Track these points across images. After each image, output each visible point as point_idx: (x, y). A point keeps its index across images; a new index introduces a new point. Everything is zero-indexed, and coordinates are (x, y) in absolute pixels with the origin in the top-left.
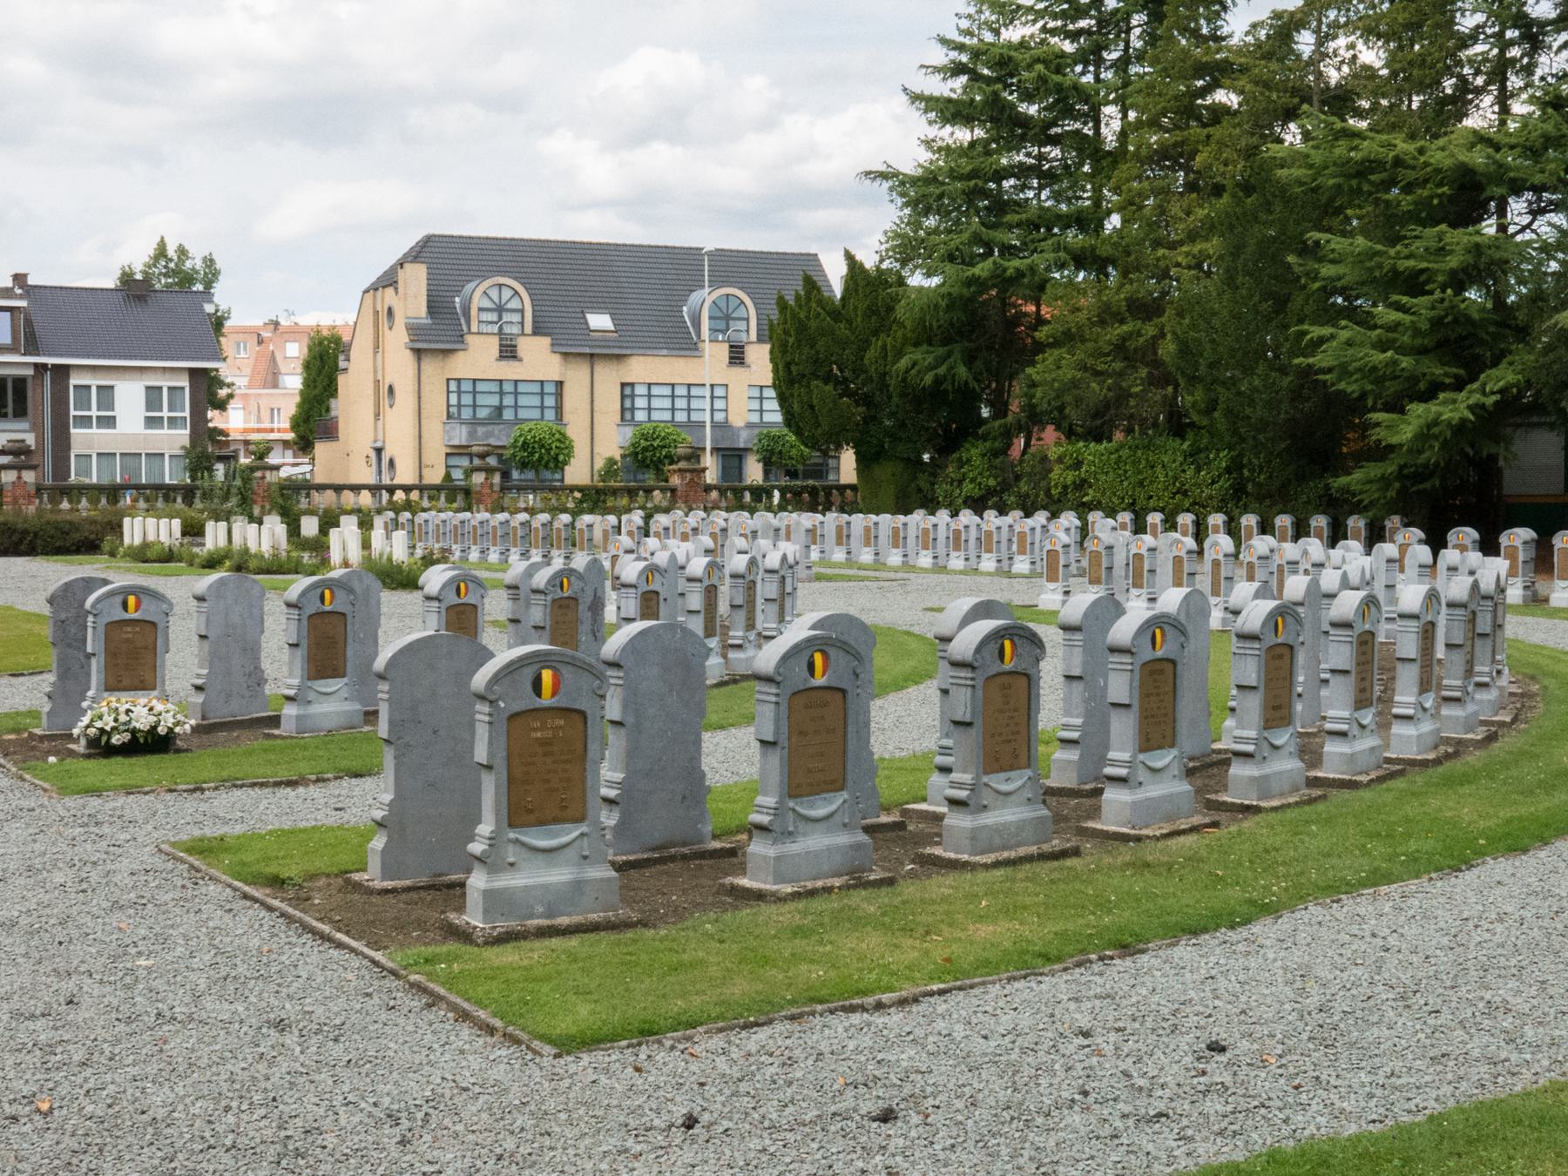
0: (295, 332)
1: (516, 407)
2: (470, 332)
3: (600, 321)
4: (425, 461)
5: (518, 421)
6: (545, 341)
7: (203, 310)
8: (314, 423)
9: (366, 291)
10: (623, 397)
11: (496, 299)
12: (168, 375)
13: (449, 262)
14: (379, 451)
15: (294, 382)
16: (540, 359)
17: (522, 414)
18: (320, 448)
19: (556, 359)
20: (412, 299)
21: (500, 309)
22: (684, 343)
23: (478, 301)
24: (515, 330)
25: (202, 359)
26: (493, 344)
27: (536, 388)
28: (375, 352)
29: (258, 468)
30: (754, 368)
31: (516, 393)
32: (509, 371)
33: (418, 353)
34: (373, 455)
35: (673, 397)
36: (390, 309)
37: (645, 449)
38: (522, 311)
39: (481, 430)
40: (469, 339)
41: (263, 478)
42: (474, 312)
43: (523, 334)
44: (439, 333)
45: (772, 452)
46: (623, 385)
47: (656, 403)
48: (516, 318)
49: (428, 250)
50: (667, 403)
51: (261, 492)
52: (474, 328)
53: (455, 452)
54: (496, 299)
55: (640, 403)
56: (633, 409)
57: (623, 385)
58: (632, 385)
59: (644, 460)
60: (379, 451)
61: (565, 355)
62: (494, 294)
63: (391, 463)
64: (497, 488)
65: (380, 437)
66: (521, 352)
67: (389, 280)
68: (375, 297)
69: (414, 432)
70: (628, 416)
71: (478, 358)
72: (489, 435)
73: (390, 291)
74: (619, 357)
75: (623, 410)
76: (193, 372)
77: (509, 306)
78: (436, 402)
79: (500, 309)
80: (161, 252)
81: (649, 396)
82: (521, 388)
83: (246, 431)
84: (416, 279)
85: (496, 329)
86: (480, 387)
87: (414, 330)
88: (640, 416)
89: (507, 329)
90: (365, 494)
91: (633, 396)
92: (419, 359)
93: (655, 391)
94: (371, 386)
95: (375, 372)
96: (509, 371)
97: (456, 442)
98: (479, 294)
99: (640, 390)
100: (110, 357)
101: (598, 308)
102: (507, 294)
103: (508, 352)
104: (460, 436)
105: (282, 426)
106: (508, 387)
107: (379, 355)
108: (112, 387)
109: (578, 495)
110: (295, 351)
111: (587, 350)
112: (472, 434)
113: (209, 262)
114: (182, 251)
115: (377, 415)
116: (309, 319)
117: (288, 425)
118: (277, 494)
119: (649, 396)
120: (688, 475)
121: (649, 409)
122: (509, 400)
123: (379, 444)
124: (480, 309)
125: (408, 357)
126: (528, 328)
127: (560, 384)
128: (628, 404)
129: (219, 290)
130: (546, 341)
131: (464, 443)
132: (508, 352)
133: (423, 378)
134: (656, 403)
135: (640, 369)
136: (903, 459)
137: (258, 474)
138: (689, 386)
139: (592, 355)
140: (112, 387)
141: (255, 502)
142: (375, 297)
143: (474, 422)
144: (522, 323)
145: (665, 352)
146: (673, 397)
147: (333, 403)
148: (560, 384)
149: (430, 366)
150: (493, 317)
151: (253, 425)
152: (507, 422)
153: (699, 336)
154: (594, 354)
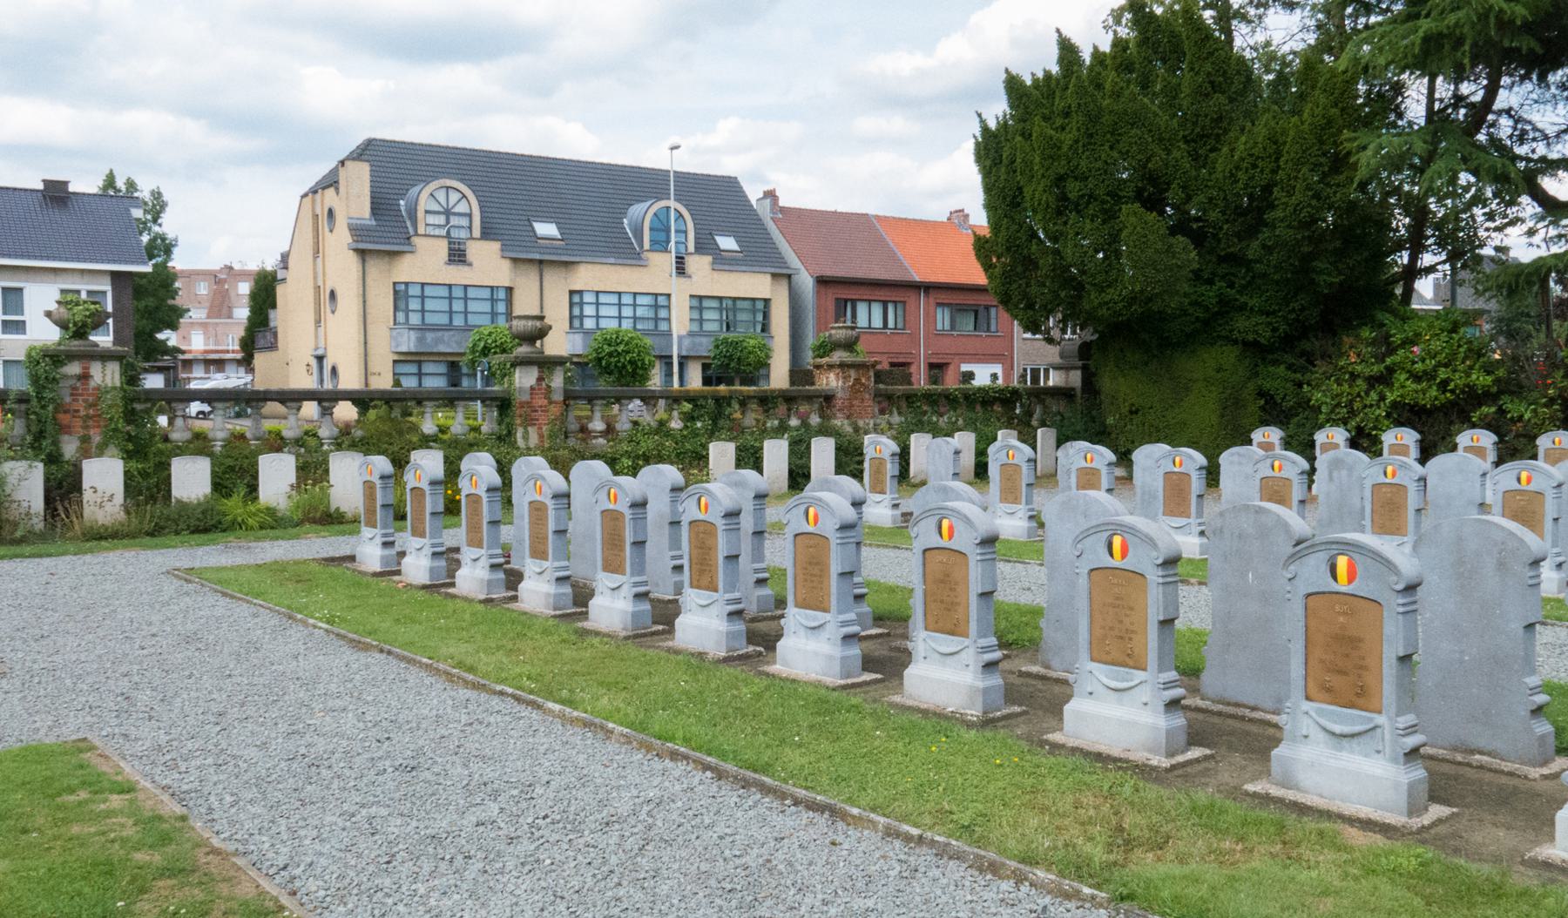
0: (243, 275)
1: (466, 313)
2: (416, 234)
3: (546, 229)
4: (371, 369)
5: (468, 328)
6: (495, 246)
7: (129, 215)
8: (259, 333)
9: (305, 195)
10: (571, 305)
11: (443, 201)
12: (86, 278)
13: (395, 170)
14: (320, 359)
15: (243, 313)
16: (489, 264)
17: (472, 320)
18: (259, 359)
19: (506, 265)
20: (355, 200)
21: (448, 213)
22: (626, 251)
23: (424, 203)
24: (463, 234)
25: (126, 262)
26: (442, 248)
27: (486, 294)
28: (315, 258)
29: (71, 357)
30: (695, 278)
31: (466, 299)
32: (457, 275)
33: (362, 254)
34: (314, 363)
35: (620, 305)
36: (331, 212)
37: (610, 355)
38: (470, 216)
39: (430, 336)
40: (415, 240)
41: (85, 377)
42: (420, 214)
43: (472, 238)
44: (384, 234)
45: (731, 358)
46: (572, 293)
47: (603, 311)
48: (464, 222)
49: (369, 151)
50: (613, 312)
51: (80, 405)
52: (421, 230)
53: (402, 359)
54: (443, 201)
55: (589, 310)
56: (582, 317)
57: (572, 293)
58: (580, 292)
59: (609, 364)
60: (320, 359)
61: (515, 260)
62: (441, 196)
63: (334, 371)
64: (558, 397)
65: (322, 344)
66: (470, 256)
67: (330, 182)
68: (313, 201)
69: (369, 327)
70: (576, 323)
71: (425, 263)
72: (437, 341)
73: (331, 192)
74: (566, 264)
75: (572, 318)
76: (116, 276)
77: (456, 210)
78: (382, 302)
79: (448, 213)
80: (110, 181)
81: (597, 304)
82: (472, 293)
83: (206, 352)
84: (359, 180)
85: (443, 232)
86: (428, 291)
87: (357, 231)
88: (589, 324)
89: (455, 234)
90: (310, 409)
91: (581, 304)
92: (364, 261)
93: (603, 298)
94: (310, 292)
95: (315, 278)
96: (457, 275)
97: (404, 349)
98: (427, 198)
99: (588, 298)
100: (16, 256)
101: (545, 219)
102: (454, 197)
103: (457, 256)
104: (408, 342)
105: (231, 344)
106: (458, 293)
107: (319, 261)
108: (21, 290)
109: (687, 407)
110: (245, 288)
111: (538, 257)
112: (420, 340)
113: (157, 195)
114: (131, 185)
115: (318, 322)
116: (253, 266)
117: (237, 348)
118: (117, 412)
119: (597, 304)
120: (853, 373)
121: (598, 317)
122: (458, 306)
123: (320, 352)
124: (427, 212)
125: (352, 260)
126: (477, 232)
127: (510, 290)
128: (576, 311)
129: (165, 219)
130: (496, 246)
131: (413, 350)
132: (457, 256)
133: (368, 280)
134: (603, 311)
135: (589, 277)
136: (1245, 344)
137: (74, 369)
138: (635, 294)
139: (541, 262)
140: (21, 290)
141: (65, 429)
142: (313, 201)
143: (424, 328)
144: (470, 228)
145: (612, 260)
146: (620, 305)
147: (272, 314)
148: (510, 290)
149: (375, 267)
150: (441, 220)
151: (211, 347)
152: (457, 329)
153: (641, 246)
154: (542, 262)
